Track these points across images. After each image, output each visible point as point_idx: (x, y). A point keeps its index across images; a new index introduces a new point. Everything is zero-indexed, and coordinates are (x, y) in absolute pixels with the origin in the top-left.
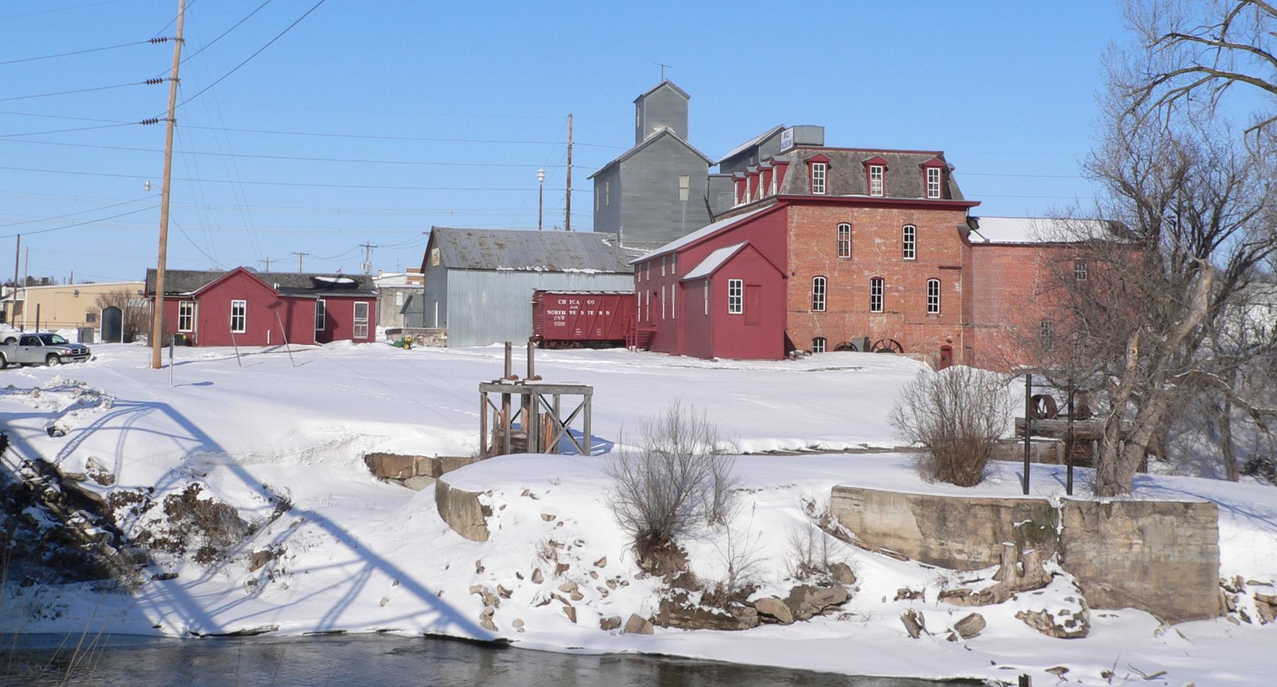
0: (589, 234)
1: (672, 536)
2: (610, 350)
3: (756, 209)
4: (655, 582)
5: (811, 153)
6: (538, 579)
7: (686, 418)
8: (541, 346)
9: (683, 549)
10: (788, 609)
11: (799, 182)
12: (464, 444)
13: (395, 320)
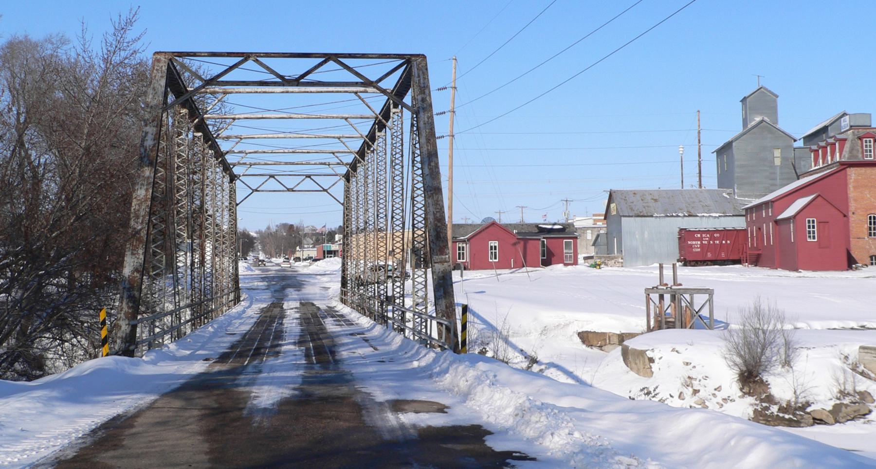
0: (714, 190)
1: (760, 374)
2: (731, 266)
3: (826, 170)
4: (750, 400)
5: (862, 132)
6: (682, 397)
7: (764, 306)
8: (685, 265)
9: (767, 381)
10: (831, 416)
11: (855, 153)
12: (637, 325)
13: (587, 249)
